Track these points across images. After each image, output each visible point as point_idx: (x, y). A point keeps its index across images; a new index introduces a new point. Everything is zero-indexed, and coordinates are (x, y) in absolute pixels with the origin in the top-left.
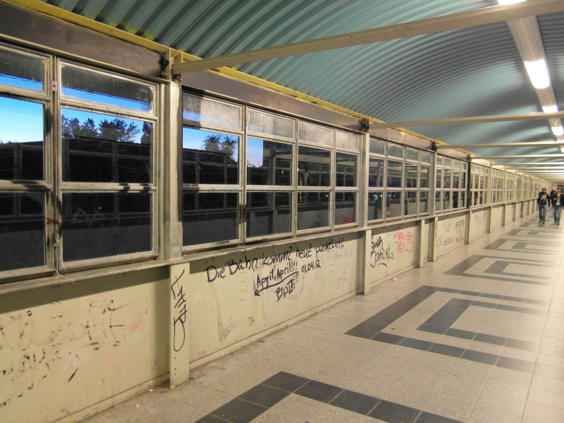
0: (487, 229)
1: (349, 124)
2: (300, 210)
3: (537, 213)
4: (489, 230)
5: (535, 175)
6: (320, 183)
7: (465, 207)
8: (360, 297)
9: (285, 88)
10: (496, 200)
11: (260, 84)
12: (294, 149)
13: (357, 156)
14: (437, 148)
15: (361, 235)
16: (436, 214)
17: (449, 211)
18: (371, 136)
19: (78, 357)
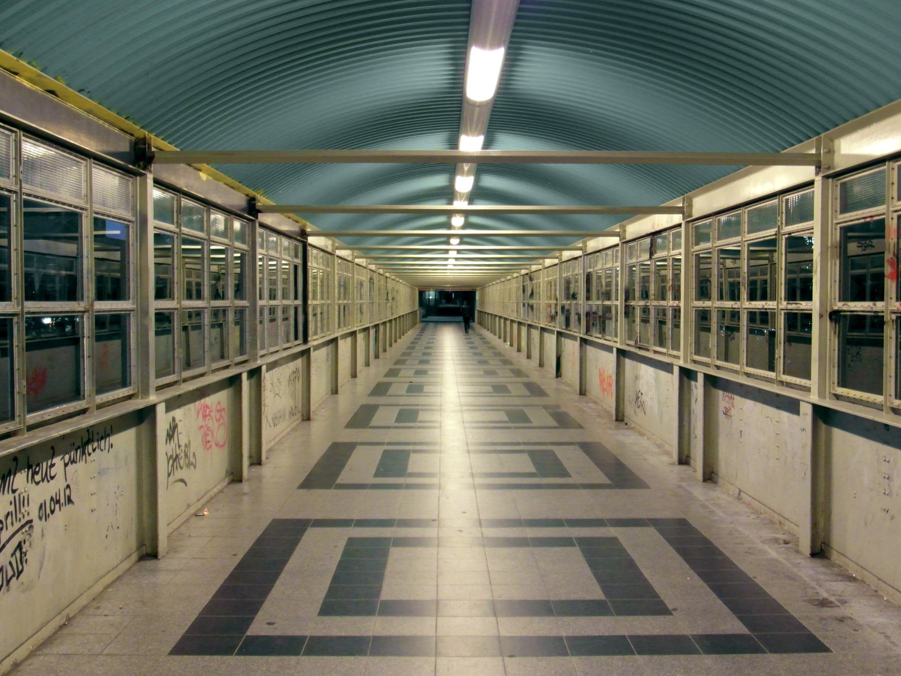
4: (369, 362)
7: (300, 341)
15: (145, 416)
16: (159, 388)
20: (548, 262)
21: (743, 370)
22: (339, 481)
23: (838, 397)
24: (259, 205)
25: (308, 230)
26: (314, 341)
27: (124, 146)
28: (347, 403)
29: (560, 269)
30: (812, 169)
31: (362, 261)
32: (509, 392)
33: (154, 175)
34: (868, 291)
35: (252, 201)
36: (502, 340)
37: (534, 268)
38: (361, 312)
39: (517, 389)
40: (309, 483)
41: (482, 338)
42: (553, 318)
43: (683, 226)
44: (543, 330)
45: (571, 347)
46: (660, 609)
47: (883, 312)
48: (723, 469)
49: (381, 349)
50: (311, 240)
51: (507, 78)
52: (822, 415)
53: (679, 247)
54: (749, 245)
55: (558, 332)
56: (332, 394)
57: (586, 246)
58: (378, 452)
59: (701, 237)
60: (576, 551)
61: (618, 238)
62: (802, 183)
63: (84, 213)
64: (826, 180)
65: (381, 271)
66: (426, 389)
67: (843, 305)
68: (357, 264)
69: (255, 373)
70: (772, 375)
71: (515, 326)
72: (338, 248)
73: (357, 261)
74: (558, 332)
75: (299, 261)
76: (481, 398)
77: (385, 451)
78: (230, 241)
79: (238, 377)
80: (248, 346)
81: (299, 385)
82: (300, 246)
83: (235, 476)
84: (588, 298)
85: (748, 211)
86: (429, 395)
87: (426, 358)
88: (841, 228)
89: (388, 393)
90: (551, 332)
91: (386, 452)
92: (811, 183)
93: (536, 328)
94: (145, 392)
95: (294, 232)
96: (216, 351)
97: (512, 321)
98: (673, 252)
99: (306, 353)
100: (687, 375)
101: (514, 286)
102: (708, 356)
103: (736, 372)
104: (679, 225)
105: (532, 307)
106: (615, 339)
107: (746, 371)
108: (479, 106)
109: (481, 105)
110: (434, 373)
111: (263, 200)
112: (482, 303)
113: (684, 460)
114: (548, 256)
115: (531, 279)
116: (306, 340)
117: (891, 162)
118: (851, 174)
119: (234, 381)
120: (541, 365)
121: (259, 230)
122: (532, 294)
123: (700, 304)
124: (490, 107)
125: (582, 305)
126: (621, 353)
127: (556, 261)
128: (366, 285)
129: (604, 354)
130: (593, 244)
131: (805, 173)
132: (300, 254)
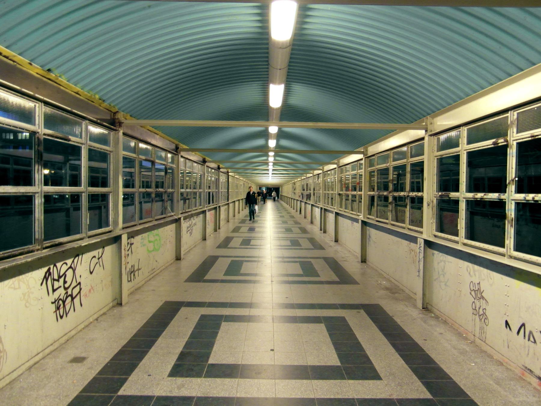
0: (203, 236)
1: (98, 117)
2: (124, 205)
3: (247, 211)
4: (229, 220)
5: (251, 181)
6: (100, 184)
7: (227, 201)
8: (178, 261)
9: (6, 49)
10: (198, 204)
11: (25, 67)
12: (136, 161)
13: (135, 160)
14: (220, 169)
17: (197, 210)
18: (124, 134)
19: (5, 328)
20: (299, 179)
21: (509, 254)
22: (228, 247)
23: (368, 218)
24: (220, 167)
25: (229, 171)
26: (230, 201)
27: (201, 159)
28: (231, 226)
29: (301, 182)
30: (424, 131)
31: (242, 179)
32: (287, 223)
33: (123, 130)
34: (486, 186)
35: (219, 166)
36: (295, 211)
37: (296, 181)
38: (241, 194)
39: (296, 230)
40: (219, 247)
41: (282, 205)
42: (300, 196)
43: (364, 160)
44: (297, 200)
45: (303, 204)
46: (318, 276)
47: (505, 199)
48: (340, 239)
49: (244, 208)
50: (230, 174)
51: (288, 90)
52: (364, 223)
53: (362, 169)
54: (352, 175)
55: (362, 221)
56: (203, 240)
57: (339, 162)
58: (240, 240)
59: (371, 165)
60: (298, 264)
61: (363, 155)
62: (520, 104)
63: (83, 146)
64: (430, 137)
65: (247, 181)
66: (253, 243)
67: (485, 195)
68: (236, 178)
69: (219, 207)
70: (332, 207)
71: (290, 199)
72: (236, 175)
73: (240, 178)
74: (362, 221)
75: (227, 180)
76: (280, 234)
77: (232, 261)
78: (137, 155)
79: (217, 207)
80: (217, 201)
81: (226, 212)
82: (227, 175)
83: (215, 230)
84: (307, 190)
85: (393, 152)
86: (259, 232)
87: (261, 209)
88: (517, 143)
89: (240, 231)
90: (332, 212)
91: (243, 240)
92: (423, 139)
93: (299, 200)
94: (204, 207)
95: (226, 172)
96: (194, 206)
97: (290, 198)
98: (359, 171)
99: (228, 204)
100: (321, 208)
101: (290, 186)
102: (387, 219)
103: (404, 228)
104: (336, 168)
105: (295, 193)
106: (335, 208)
107: (391, 223)
108: (276, 110)
109: (277, 109)
110: (261, 222)
111: (221, 166)
112: (282, 192)
113: (321, 230)
114: (303, 175)
115: (295, 184)
116: (228, 201)
117: (463, 127)
118: (523, 107)
119: (215, 208)
120: (305, 217)
121: (220, 173)
122: (295, 189)
123: (324, 192)
124: (279, 111)
125: (305, 193)
126: (312, 205)
127: (300, 179)
128: (243, 186)
129: (309, 205)
130: (327, 167)
131: (360, 156)
132: (227, 178)
